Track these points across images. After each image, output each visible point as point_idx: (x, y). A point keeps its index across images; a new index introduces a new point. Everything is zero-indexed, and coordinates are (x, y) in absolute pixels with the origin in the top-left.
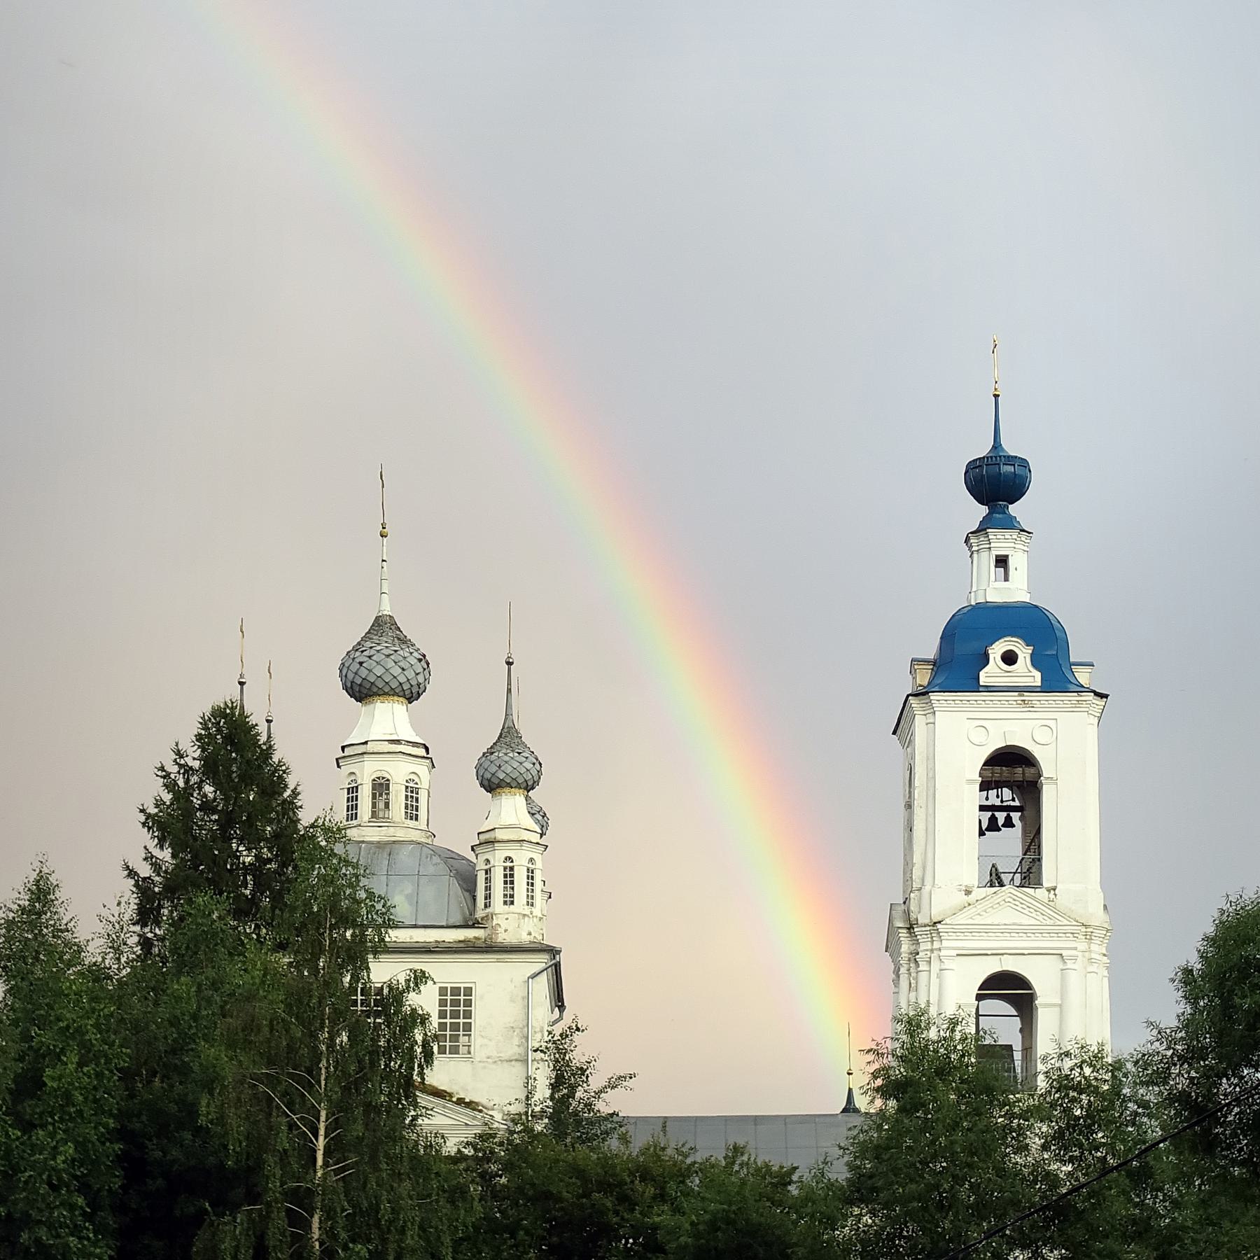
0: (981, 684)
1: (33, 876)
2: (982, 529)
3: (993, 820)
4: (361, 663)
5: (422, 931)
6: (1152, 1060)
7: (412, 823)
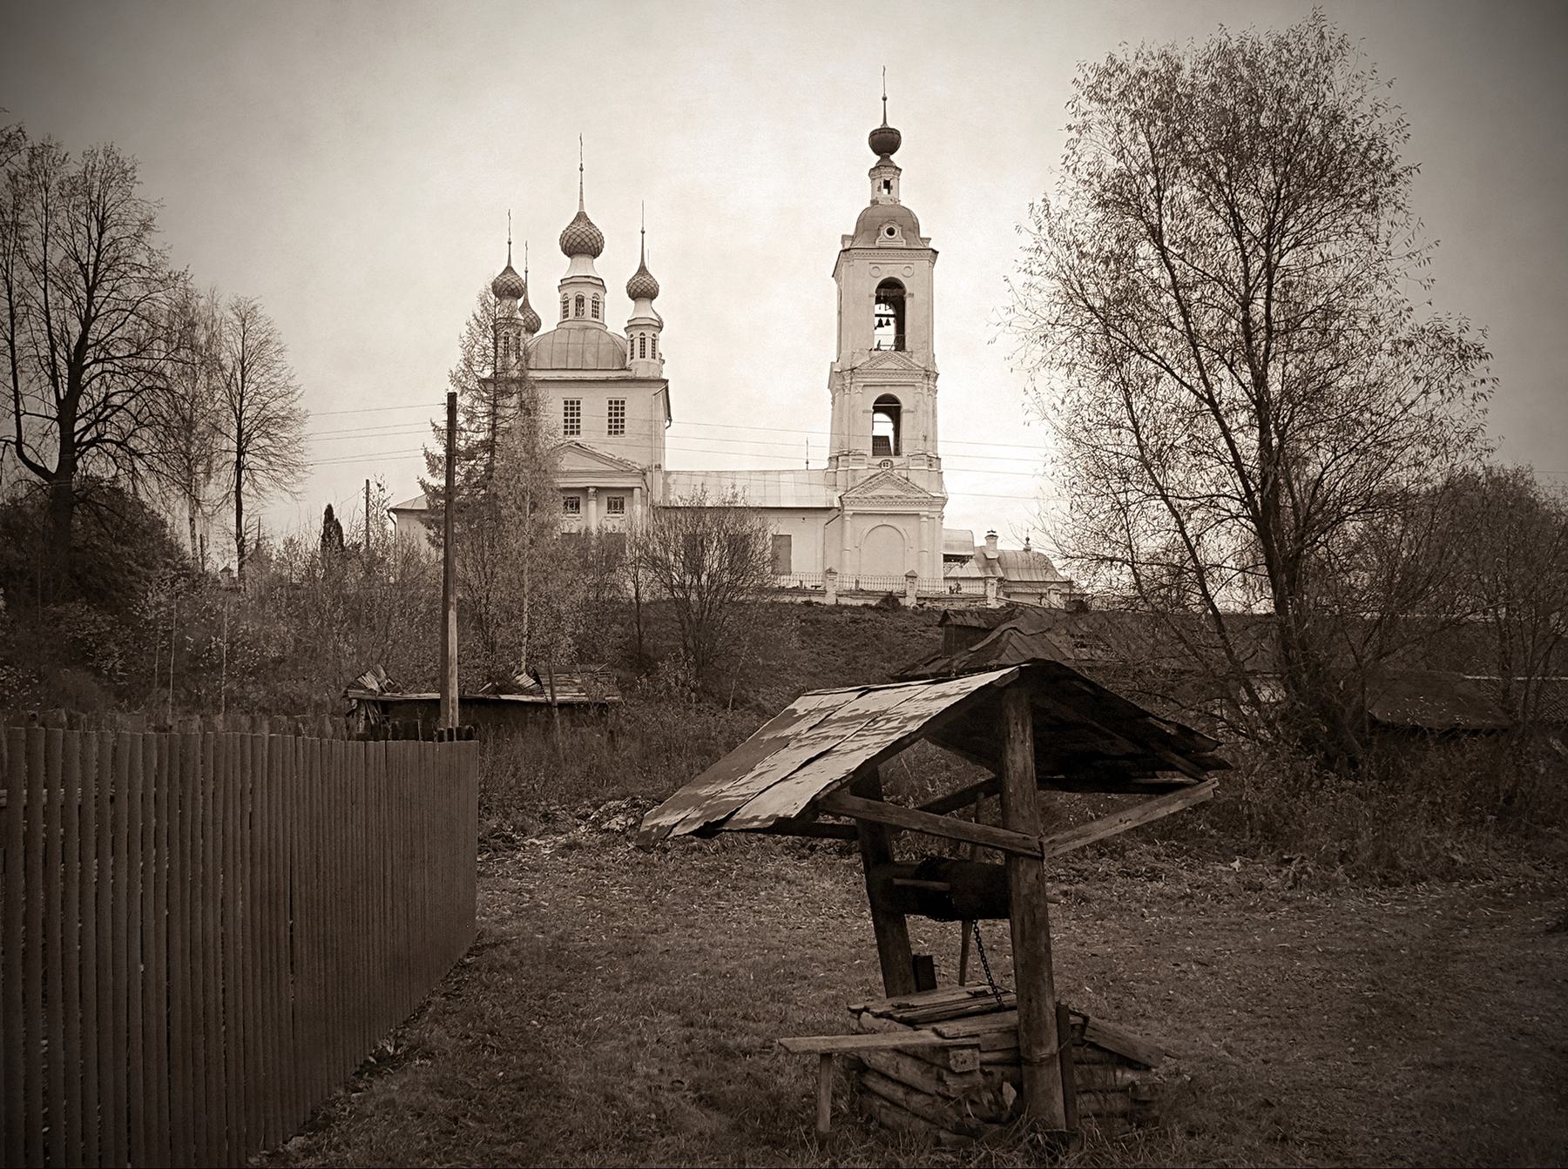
0: (922, 236)
2: (877, 167)
3: (880, 321)
5: (570, 372)
6: (1346, 498)
7: (595, 320)
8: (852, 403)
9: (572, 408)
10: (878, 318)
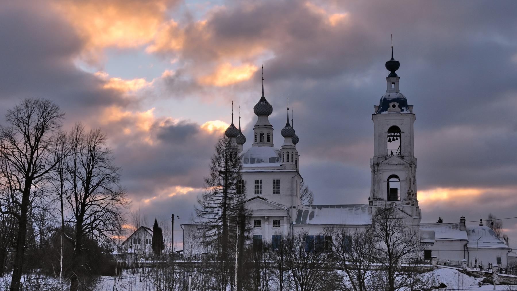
1: (439, 218)
3: (390, 139)
4: (258, 108)
8: (378, 179)
9: (258, 183)
10: (389, 137)
